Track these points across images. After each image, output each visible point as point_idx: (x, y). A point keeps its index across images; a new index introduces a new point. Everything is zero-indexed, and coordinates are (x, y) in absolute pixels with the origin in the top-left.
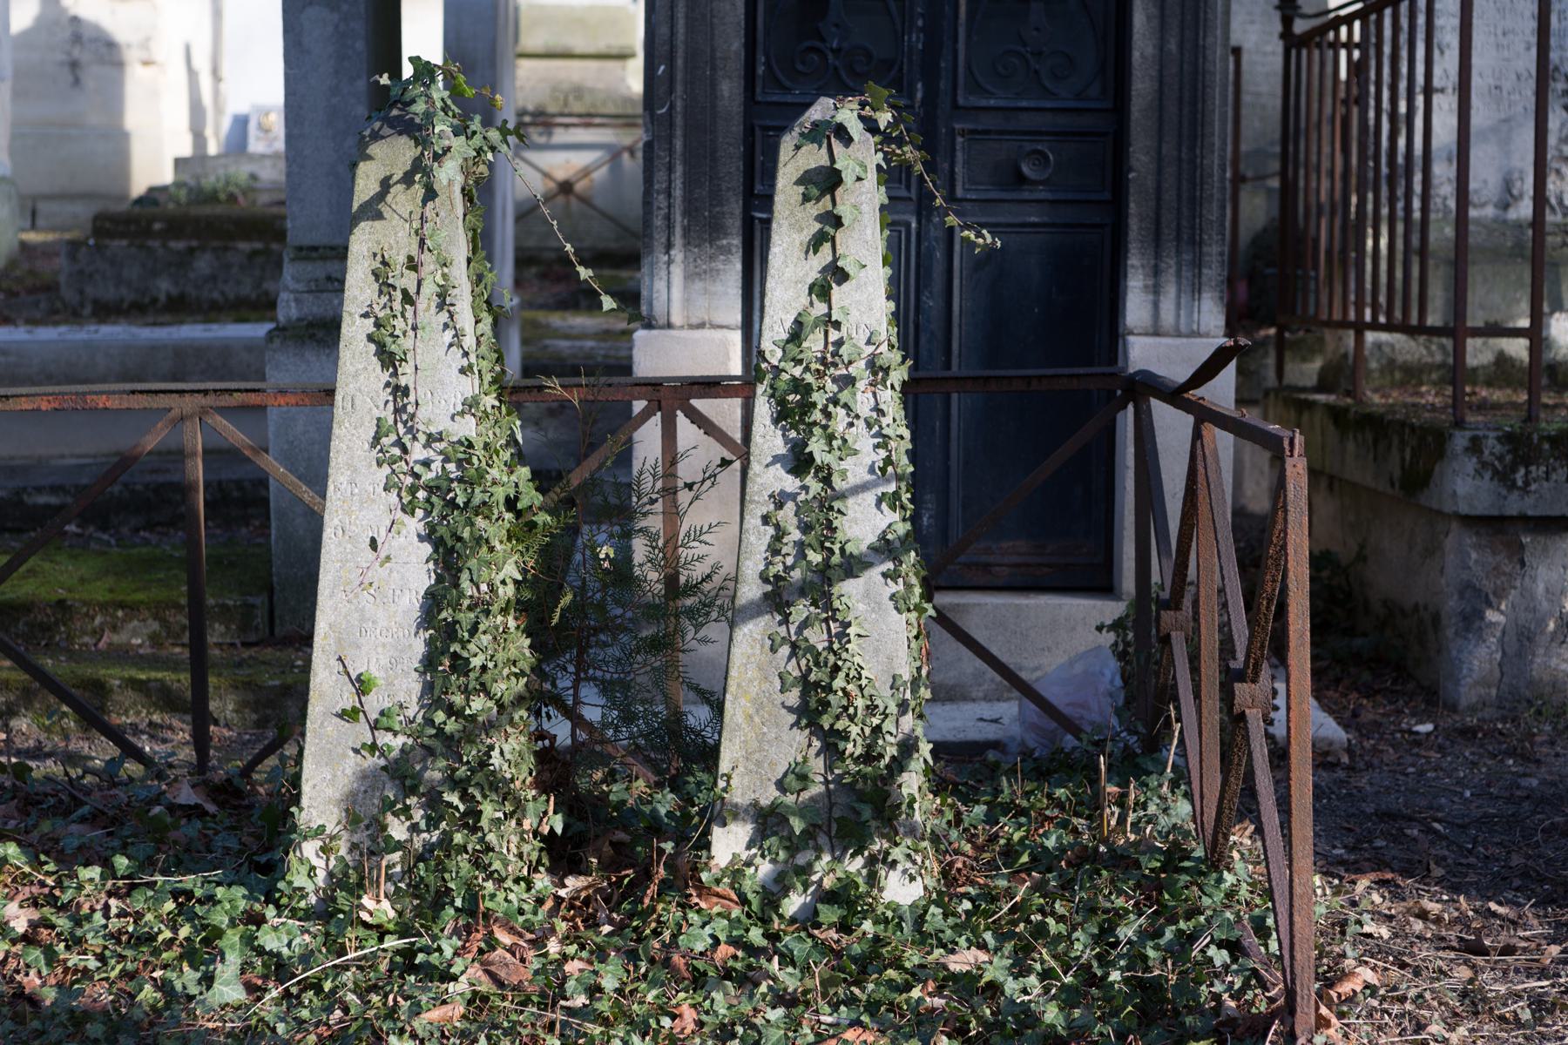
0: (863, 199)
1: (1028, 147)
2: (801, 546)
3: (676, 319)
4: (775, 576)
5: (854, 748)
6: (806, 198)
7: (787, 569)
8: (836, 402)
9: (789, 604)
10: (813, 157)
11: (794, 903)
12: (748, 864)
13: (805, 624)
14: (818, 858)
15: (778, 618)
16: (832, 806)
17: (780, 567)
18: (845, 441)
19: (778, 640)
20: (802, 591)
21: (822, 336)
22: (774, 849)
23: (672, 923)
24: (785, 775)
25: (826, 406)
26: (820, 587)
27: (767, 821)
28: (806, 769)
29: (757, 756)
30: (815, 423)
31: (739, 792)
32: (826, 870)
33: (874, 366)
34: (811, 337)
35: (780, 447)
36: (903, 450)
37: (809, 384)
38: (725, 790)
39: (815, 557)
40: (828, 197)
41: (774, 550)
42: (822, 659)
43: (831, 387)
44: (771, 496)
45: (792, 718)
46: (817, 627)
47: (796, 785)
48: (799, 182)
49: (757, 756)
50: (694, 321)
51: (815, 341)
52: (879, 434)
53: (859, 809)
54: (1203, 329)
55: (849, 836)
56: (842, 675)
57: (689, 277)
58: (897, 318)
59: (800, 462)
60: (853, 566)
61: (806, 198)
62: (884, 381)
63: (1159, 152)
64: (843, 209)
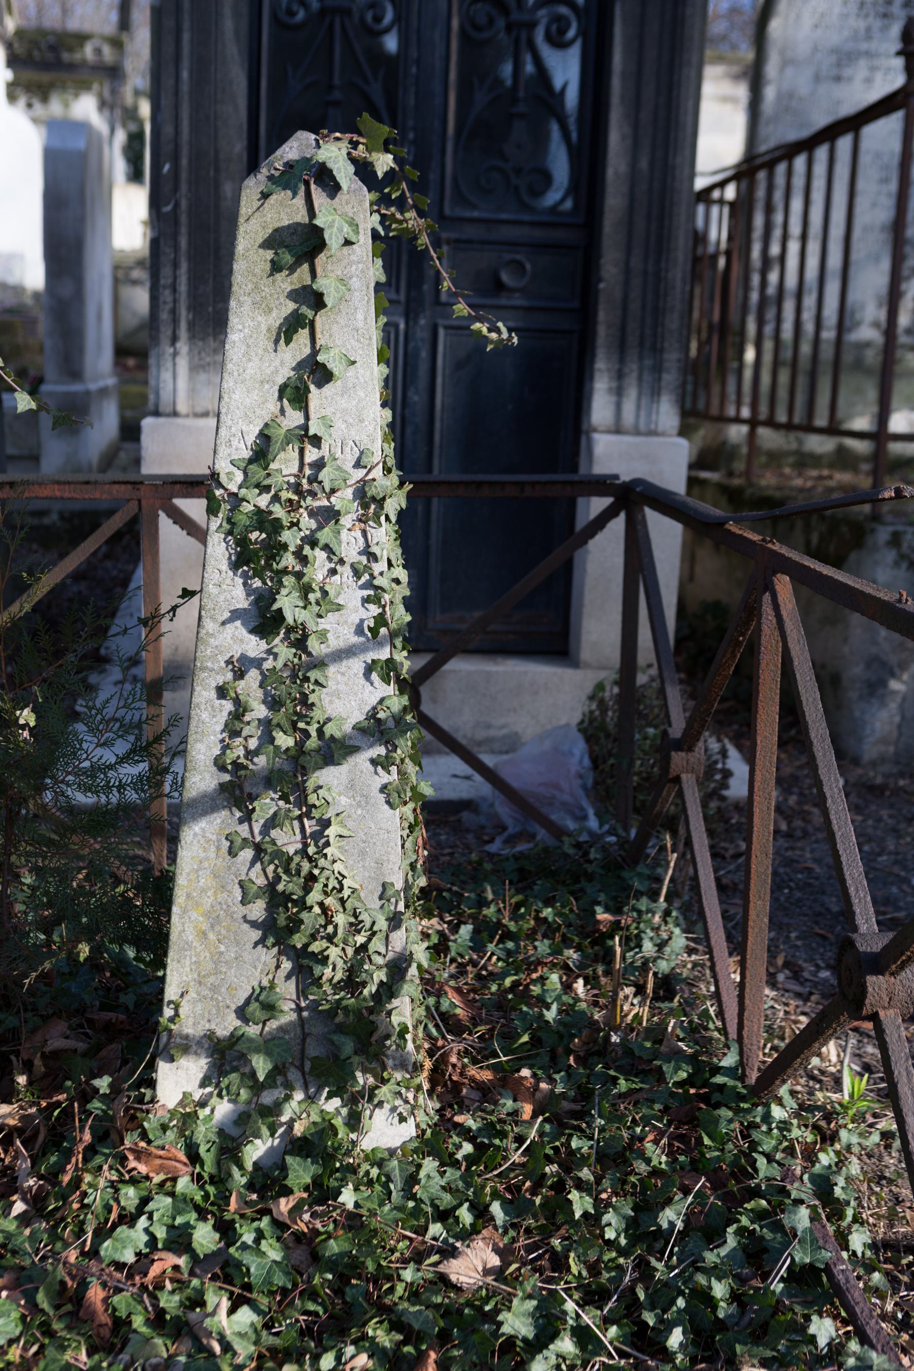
0: (353, 275)
1: (507, 257)
2: (267, 726)
3: (182, 407)
4: (234, 763)
5: (333, 971)
6: (276, 267)
7: (250, 754)
8: (313, 543)
9: (252, 798)
10: (286, 210)
11: (256, 1150)
12: (202, 1104)
13: (272, 823)
14: (288, 1098)
15: (238, 814)
16: (305, 1036)
17: (241, 752)
18: (325, 593)
19: (238, 841)
20: (270, 780)
21: (296, 454)
22: (234, 1089)
23: (98, 1205)
24: (248, 1002)
25: (301, 548)
26: (292, 777)
27: (225, 1056)
28: (272, 998)
29: (212, 979)
30: (285, 571)
31: (191, 1021)
32: (299, 1111)
33: (362, 495)
34: (282, 455)
35: (239, 598)
36: (398, 599)
37: (278, 520)
38: (172, 1020)
39: (285, 741)
40: (306, 266)
41: (233, 729)
42: (293, 866)
43: (308, 523)
44: (228, 662)
45: (256, 935)
46: (287, 827)
47: (260, 1014)
48: (267, 244)
49: (212, 979)
50: (199, 409)
51: (287, 461)
52: (369, 585)
53: (338, 1042)
54: (660, 429)
55: (330, 1074)
56: (318, 887)
57: (195, 369)
58: (398, 431)
59: (265, 620)
60: (334, 751)
61: (276, 267)
62: (377, 517)
63: (627, 262)
64: (324, 284)
